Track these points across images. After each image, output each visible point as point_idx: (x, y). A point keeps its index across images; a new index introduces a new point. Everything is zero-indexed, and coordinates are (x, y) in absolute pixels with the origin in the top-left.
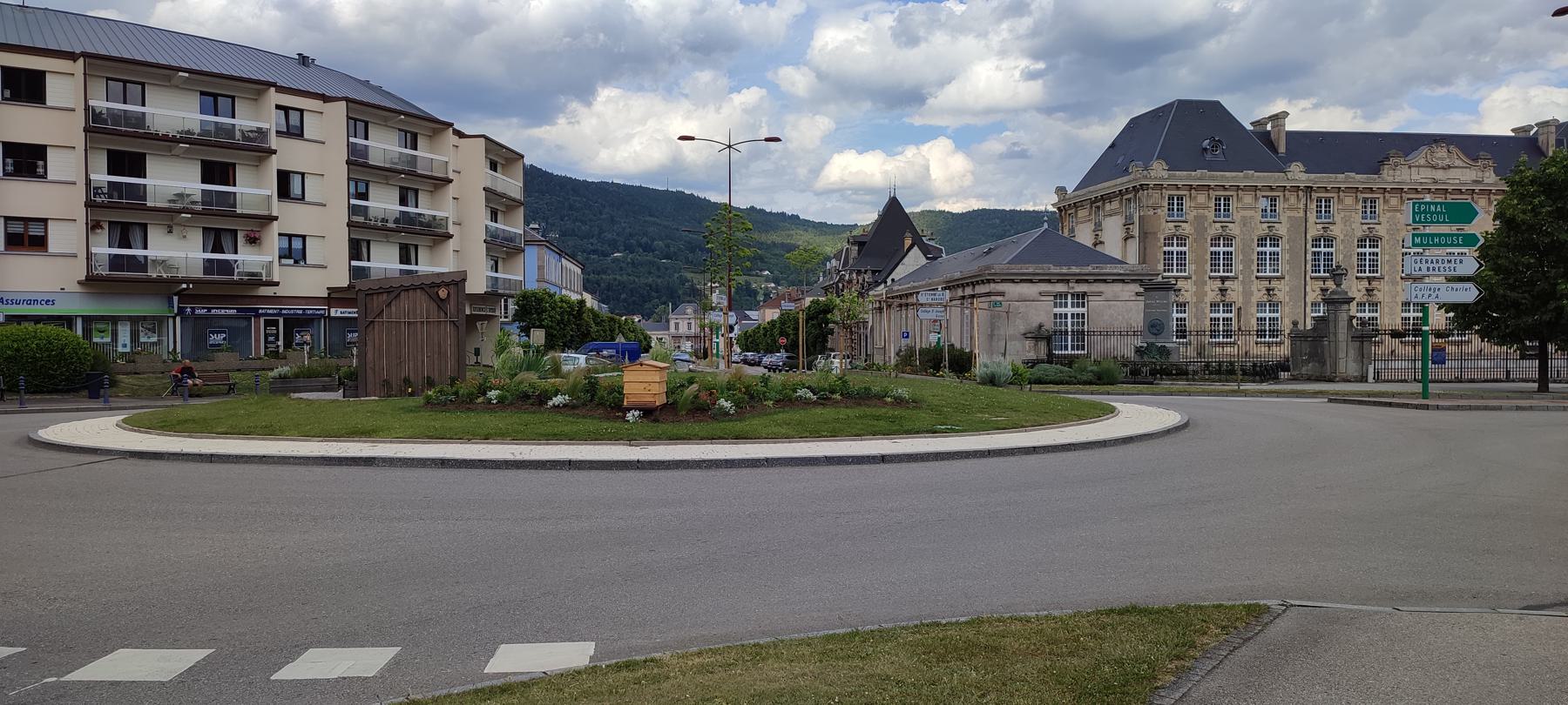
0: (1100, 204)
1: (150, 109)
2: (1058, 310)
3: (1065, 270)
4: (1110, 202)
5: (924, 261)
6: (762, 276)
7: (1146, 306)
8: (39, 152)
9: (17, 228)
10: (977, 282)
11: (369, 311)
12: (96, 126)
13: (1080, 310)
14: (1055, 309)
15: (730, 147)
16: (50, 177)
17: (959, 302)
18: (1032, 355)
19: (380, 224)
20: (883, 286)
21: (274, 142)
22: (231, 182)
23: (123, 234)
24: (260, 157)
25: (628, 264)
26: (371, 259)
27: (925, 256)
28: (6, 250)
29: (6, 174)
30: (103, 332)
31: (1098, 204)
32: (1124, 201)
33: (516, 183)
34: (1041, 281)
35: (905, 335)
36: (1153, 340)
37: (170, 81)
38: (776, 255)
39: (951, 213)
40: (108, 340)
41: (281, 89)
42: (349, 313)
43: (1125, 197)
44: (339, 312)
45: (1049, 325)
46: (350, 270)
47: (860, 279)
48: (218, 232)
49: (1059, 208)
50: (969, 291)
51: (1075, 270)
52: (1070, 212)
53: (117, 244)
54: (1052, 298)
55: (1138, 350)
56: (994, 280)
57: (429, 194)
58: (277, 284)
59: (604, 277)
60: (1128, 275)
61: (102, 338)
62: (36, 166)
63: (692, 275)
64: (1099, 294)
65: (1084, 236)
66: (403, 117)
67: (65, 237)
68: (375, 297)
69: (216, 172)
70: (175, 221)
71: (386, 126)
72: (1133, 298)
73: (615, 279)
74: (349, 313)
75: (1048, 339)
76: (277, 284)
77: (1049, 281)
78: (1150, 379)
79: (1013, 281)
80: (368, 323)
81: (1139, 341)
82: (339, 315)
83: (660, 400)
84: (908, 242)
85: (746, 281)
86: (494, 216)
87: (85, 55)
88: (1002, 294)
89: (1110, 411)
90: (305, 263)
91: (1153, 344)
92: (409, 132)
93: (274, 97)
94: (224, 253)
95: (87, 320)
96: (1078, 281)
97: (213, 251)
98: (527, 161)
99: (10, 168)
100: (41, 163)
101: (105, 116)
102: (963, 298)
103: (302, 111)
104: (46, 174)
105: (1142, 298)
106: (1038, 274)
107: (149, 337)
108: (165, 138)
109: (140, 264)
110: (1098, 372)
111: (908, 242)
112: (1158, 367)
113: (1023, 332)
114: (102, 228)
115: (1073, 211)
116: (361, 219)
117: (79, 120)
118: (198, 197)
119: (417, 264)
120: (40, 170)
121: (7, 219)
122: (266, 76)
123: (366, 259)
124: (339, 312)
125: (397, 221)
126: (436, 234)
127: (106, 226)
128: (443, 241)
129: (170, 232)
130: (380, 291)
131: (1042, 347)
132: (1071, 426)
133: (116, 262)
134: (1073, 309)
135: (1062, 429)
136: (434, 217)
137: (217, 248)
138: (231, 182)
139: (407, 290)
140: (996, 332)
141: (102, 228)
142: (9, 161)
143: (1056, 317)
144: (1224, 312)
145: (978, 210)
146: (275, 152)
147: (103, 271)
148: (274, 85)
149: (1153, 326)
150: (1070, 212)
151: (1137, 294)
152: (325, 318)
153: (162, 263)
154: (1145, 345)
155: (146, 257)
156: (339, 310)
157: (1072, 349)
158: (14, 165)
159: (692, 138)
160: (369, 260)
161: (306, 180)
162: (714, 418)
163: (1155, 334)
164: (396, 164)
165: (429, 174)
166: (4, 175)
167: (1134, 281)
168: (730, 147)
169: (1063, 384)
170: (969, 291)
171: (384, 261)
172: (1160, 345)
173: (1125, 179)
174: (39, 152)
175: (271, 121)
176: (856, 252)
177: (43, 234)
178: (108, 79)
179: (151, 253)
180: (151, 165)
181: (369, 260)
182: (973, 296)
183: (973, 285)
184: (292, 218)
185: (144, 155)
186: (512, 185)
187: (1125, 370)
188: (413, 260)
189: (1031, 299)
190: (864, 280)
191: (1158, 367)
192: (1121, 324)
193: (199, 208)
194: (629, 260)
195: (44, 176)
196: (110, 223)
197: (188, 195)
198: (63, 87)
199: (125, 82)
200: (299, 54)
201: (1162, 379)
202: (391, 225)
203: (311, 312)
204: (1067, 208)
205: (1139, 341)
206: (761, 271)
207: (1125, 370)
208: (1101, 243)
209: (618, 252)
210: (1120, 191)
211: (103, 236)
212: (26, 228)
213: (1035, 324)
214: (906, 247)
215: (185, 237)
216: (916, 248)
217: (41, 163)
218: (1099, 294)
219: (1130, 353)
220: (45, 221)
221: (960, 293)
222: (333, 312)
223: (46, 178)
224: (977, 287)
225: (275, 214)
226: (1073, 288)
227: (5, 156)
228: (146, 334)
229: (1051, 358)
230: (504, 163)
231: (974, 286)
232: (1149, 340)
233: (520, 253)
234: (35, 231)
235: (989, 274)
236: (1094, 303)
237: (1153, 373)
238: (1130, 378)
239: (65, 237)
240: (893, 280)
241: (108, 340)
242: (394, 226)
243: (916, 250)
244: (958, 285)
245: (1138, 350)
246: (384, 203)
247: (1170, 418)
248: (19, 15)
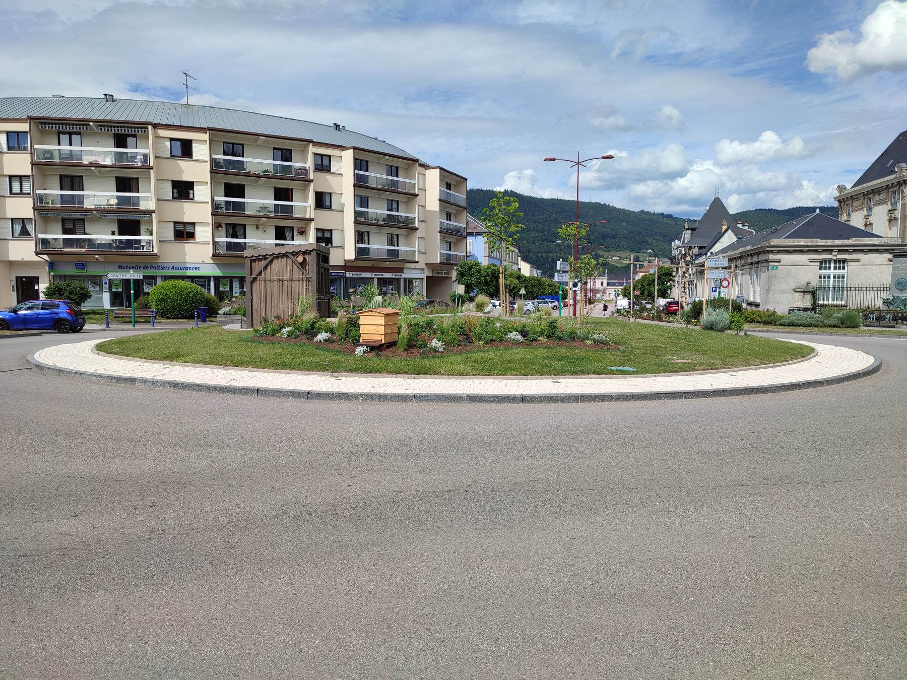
0: (871, 196)
1: (246, 158)
2: (823, 272)
3: (829, 242)
4: (879, 194)
5: (735, 239)
6: (647, 253)
7: (894, 269)
8: (190, 185)
9: (180, 228)
10: (760, 252)
11: (253, 271)
12: (216, 167)
13: (841, 272)
14: (820, 271)
15: (578, 164)
16: (196, 199)
17: (749, 267)
18: (800, 305)
19: (374, 222)
20: (704, 257)
21: (311, 176)
22: (291, 200)
23: (235, 230)
24: (305, 184)
25: (565, 247)
26: (370, 243)
27: (736, 236)
28: (175, 240)
29: (174, 198)
30: (118, 285)
31: (869, 196)
32: (890, 192)
33: (462, 196)
34: (809, 251)
35: (714, 289)
36: (899, 294)
37: (256, 142)
38: (656, 240)
39: (777, 210)
40: (228, 289)
41: (317, 144)
42: (358, 275)
43: (891, 190)
44: (351, 274)
45: (815, 283)
46: (355, 250)
47: (691, 252)
48: (235, 226)
49: (840, 201)
50: (755, 259)
51: (838, 242)
52: (847, 203)
53: (230, 236)
54: (819, 263)
55: (886, 302)
56: (772, 251)
57: (405, 203)
58: (417, 262)
59: (550, 254)
60: (882, 246)
61: (117, 289)
62: (189, 193)
63: (603, 253)
64: (858, 261)
65: (857, 220)
66: (387, 157)
67: (204, 233)
68: (257, 262)
69: (283, 194)
70: (260, 223)
71: (379, 163)
72: (886, 263)
73: (557, 256)
74: (358, 275)
75: (813, 293)
76: (417, 262)
77: (816, 251)
78: (892, 323)
79: (787, 252)
80: (252, 279)
81: (888, 294)
82: (351, 276)
83: (382, 339)
84: (724, 228)
85: (637, 256)
86: (449, 216)
87: (210, 129)
88: (779, 261)
89: (804, 353)
90: (332, 246)
91: (898, 297)
92: (394, 166)
93: (312, 149)
94: (238, 238)
95: (217, 279)
96: (840, 251)
97: (232, 237)
98: (471, 185)
99: (176, 195)
100: (191, 192)
101: (222, 163)
102: (752, 263)
103: (330, 156)
104: (194, 197)
105: (891, 263)
106: (807, 246)
107: (95, 288)
108: (254, 175)
109: (242, 247)
110: (842, 318)
111: (724, 228)
112: (900, 315)
113: (794, 288)
114: (221, 227)
115: (850, 202)
116: (362, 219)
117: (208, 166)
118: (272, 209)
119: (398, 246)
120: (191, 196)
121: (175, 223)
122: (327, 140)
123: (367, 243)
124: (351, 274)
125: (384, 220)
126: (409, 227)
127: (224, 226)
128: (414, 232)
129: (257, 228)
130: (259, 259)
131: (808, 299)
132: (763, 368)
133: (230, 246)
134: (835, 271)
135: (733, 374)
136: (407, 217)
137: (235, 236)
138: (291, 200)
139: (278, 256)
140: (772, 288)
141: (221, 227)
142: (176, 191)
143: (820, 277)
144: (835, 268)
145: (797, 208)
146: (312, 181)
147: (223, 250)
148: (417, 161)
149: (899, 283)
150: (847, 203)
151: (890, 260)
152: (343, 278)
153: (254, 247)
154: (892, 298)
155: (245, 243)
156: (352, 273)
157: (832, 300)
158: (178, 193)
159: (554, 160)
160: (369, 244)
161: (332, 197)
162: (425, 355)
163: (901, 290)
164: (385, 186)
165: (404, 191)
166: (173, 199)
167: (886, 251)
168: (578, 164)
169: (803, 326)
170: (755, 259)
171: (378, 245)
172: (904, 298)
173: (893, 177)
174: (190, 185)
175: (310, 164)
176: (689, 235)
177: (72, 227)
178: (224, 143)
179: (248, 241)
180: (247, 191)
181: (369, 244)
182: (758, 262)
183: (758, 254)
184: (324, 219)
185: (244, 185)
186: (460, 197)
187: (871, 317)
188: (396, 244)
189: (801, 264)
190: (693, 253)
191: (900, 315)
192: (874, 282)
193: (273, 215)
194: (566, 244)
195: (330, 208)
196: (227, 224)
197: (266, 208)
198: (201, 151)
199: (233, 144)
200: (334, 124)
201: (902, 324)
202: (381, 222)
203: (335, 274)
204: (846, 201)
205: (888, 294)
206: (646, 250)
207: (871, 317)
208: (871, 224)
209: (560, 240)
210: (887, 186)
211: (223, 231)
212: (323, 235)
213: (804, 283)
214: (723, 230)
215: (265, 231)
216: (730, 231)
217: (191, 192)
218: (858, 261)
219: (880, 304)
220: (194, 224)
221: (749, 260)
222: (348, 274)
223: (194, 200)
224: (760, 255)
225: (417, 226)
226: (836, 256)
227: (173, 188)
228: (93, 286)
229: (814, 307)
230: (455, 184)
231: (758, 255)
232: (896, 294)
233: (463, 239)
234: (327, 235)
235: (768, 247)
236: (851, 268)
237: (895, 319)
238: (876, 323)
239: (204, 233)
240: (711, 253)
241: (228, 289)
242: (383, 223)
243: (730, 232)
244: (748, 255)
245: (886, 302)
246: (378, 210)
247: (860, 361)
248: (184, 109)
